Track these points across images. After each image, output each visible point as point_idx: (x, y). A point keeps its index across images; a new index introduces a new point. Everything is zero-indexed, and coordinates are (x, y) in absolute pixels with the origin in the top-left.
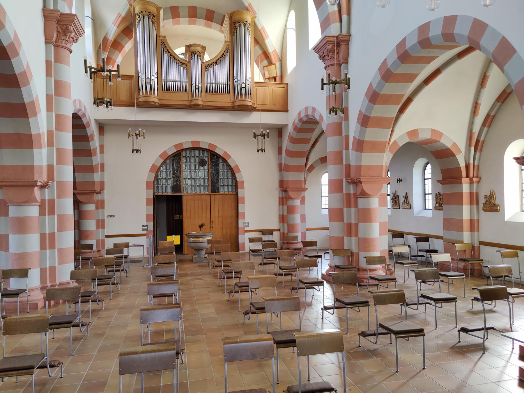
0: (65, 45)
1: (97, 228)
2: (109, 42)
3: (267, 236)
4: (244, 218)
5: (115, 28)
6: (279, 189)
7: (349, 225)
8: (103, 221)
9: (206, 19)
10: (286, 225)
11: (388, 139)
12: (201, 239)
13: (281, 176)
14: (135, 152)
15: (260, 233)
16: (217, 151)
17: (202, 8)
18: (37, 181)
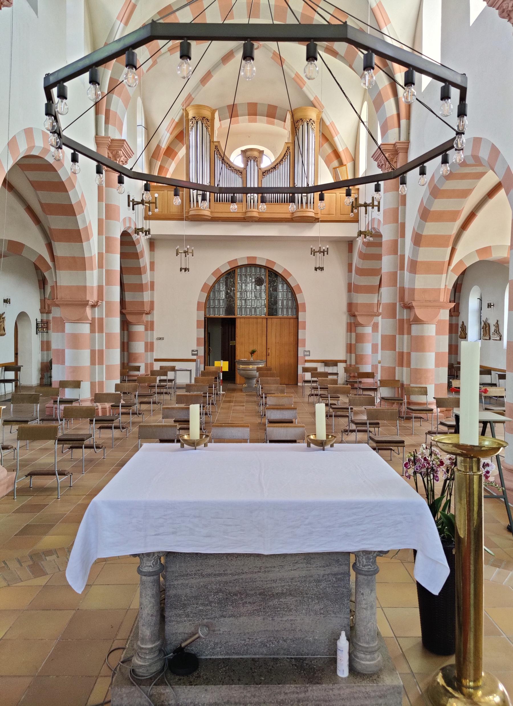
1: (146, 351)
2: (162, 149)
3: (331, 368)
4: (304, 346)
5: (168, 134)
6: (347, 313)
7: (401, 354)
8: (152, 344)
10: (353, 355)
11: (447, 258)
12: (251, 367)
13: (350, 297)
14: (183, 270)
15: (323, 364)
16: (275, 268)
17: (263, 104)
18: (88, 301)
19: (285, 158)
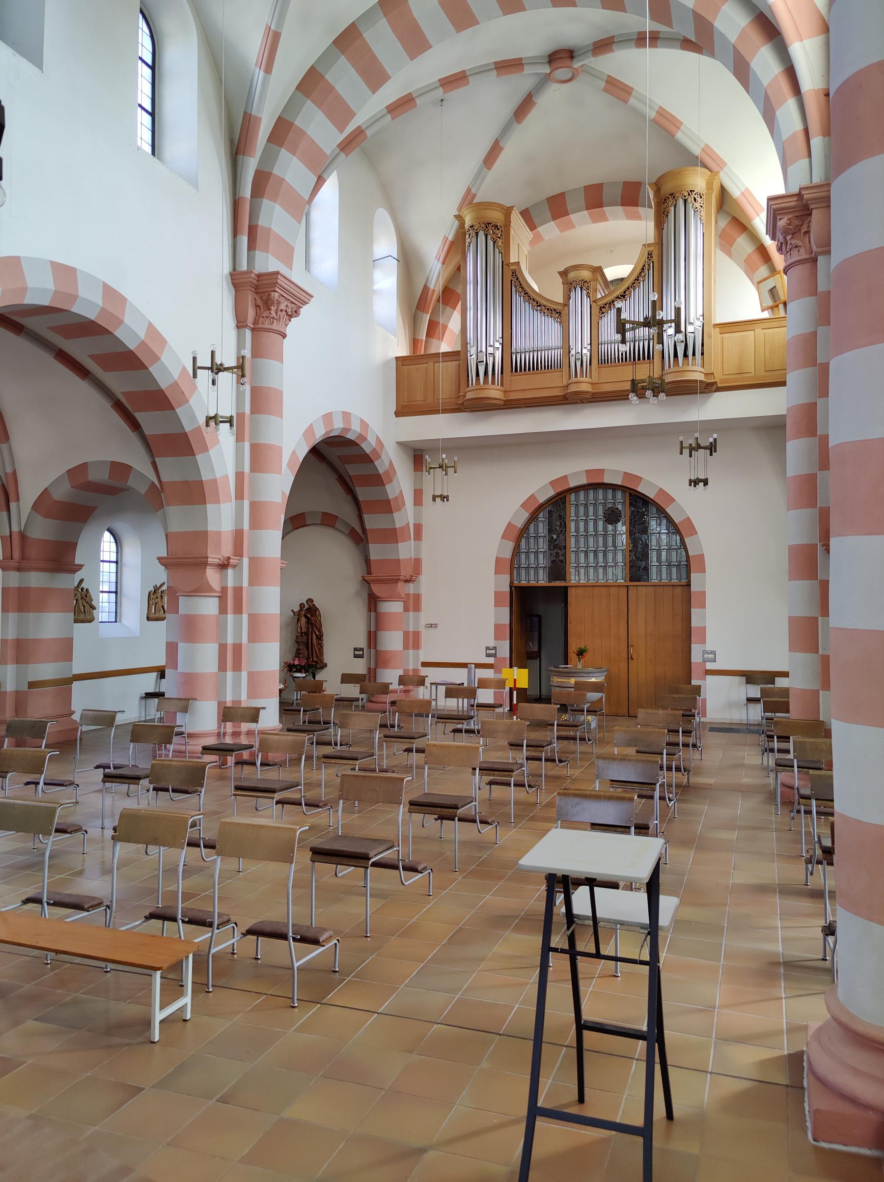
0: (269, 326)
1: (406, 647)
4: (703, 641)
5: (440, 265)
8: (417, 635)
9: (622, 205)
19: (643, 274)
